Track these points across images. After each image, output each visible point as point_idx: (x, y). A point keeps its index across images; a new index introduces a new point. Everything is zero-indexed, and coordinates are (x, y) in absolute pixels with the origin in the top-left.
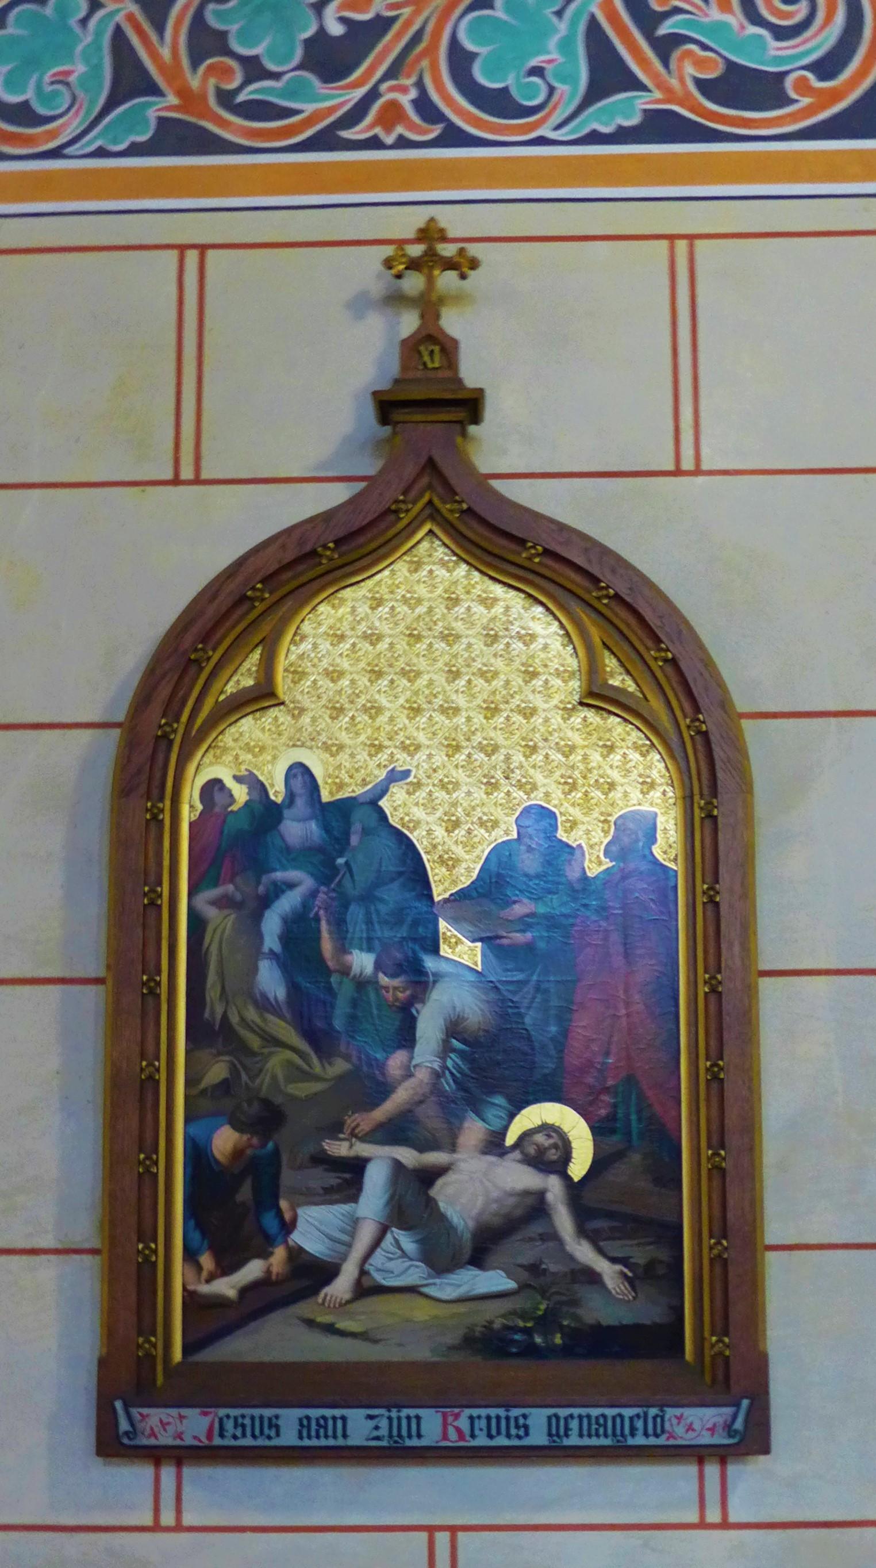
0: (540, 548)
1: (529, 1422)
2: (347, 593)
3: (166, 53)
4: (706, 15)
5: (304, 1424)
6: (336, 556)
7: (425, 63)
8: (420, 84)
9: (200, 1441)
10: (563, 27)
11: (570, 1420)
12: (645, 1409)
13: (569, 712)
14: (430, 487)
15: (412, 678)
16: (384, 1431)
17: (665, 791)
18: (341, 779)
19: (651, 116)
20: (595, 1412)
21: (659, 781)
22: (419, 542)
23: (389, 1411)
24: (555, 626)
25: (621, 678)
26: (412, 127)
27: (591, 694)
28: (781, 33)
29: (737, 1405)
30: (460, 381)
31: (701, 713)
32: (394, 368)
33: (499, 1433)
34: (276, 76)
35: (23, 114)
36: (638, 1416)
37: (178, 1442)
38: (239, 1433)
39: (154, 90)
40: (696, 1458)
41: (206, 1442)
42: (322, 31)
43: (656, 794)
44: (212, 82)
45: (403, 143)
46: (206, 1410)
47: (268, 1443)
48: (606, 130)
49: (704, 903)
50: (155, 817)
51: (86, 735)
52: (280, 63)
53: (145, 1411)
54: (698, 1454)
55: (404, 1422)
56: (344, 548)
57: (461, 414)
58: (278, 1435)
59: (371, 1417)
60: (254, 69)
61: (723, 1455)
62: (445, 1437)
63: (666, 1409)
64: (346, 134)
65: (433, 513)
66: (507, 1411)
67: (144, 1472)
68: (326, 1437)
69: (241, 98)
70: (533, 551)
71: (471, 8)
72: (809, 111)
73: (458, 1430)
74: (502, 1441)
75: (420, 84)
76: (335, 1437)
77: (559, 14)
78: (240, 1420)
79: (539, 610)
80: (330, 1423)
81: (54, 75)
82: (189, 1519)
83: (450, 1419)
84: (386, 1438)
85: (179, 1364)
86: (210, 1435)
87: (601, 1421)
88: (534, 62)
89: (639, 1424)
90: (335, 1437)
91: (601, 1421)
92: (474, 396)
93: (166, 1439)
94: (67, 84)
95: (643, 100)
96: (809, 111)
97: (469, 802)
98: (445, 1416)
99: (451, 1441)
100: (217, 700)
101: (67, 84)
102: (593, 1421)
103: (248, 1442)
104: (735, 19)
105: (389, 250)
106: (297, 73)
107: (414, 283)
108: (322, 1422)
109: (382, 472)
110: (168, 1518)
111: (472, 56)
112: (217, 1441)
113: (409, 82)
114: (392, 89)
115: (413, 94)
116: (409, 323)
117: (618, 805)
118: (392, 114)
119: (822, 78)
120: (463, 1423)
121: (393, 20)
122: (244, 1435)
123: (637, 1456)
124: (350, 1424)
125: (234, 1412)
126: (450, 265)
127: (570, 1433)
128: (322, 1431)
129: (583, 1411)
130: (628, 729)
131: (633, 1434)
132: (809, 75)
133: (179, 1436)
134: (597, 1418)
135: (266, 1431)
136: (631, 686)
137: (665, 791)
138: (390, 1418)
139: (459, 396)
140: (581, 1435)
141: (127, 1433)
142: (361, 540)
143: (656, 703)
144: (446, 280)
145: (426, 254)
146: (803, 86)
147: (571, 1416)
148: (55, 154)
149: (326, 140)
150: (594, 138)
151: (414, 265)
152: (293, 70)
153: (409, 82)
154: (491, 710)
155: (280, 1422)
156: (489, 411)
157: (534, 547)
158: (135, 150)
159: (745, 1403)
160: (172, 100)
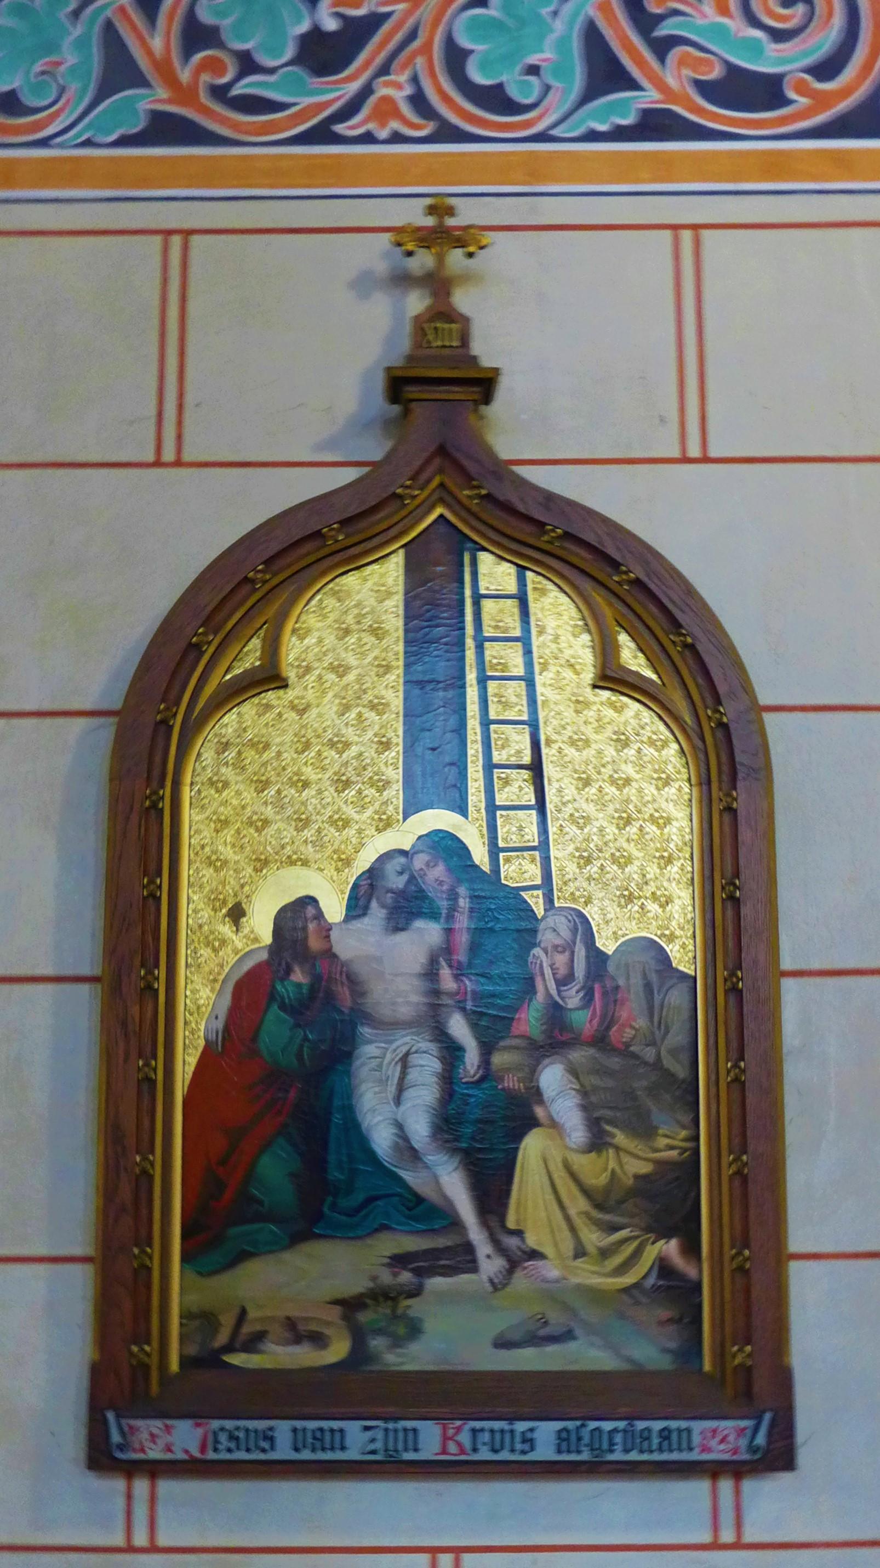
3: (157, 43)
5: (563, 1439)
8: (415, 80)
14: (441, 471)
15: (220, 789)
16: (379, 1445)
19: (647, 114)
20: (312, 1425)
28: (778, 36)
29: (759, 1419)
31: (722, 705)
32: (405, 345)
34: (272, 71)
37: (169, 1456)
41: (196, 1453)
44: (205, 78)
45: (397, 138)
46: (199, 1421)
48: (603, 127)
49: (723, 900)
50: (154, 805)
51: (81, 722)
53: (133, 1422)
54: (714, 1470)
58: (273, 1448)
59: (367, 1428)
60: (248, 65)
62: (444, 1452)
64: (340, 128)
67: (700, 1488)
69: (236, 91)
70: (553, 534)
71: (465, 8)
73: (459, 1444)
74: (505, 1455)
75: (415, 80)
77: (555, 13)
83: (451, 1432)
84: (382, 1452)
86: (203, 1449)
88: (533, 59)
91: (564, 1445)
92: (490, 375)
93: (155, 1453)
98: (445, 1429)
103: (242, 1455)
105: (428, 201)
106: (290, 68)
107: (423, 261)
109: (388, 458)
110: (727, 1536)
111: (467, 53)
112: (211, 1455)
113: (403, 78)
114: (387, 84)
115: (408, 90)
117: (632, 801)
118: (387, 110)
120: (465, 1438)
124: (421, 1437)
125: (229, 1424)
132: (807, 77)
133: (169, 1449)
136: (649, 674)
144: (456, 257)
147: (615, 1430)
148: (44, 143)
150: (593, 136)
153: (403, 78)
154: (343, 784)
155: (536, 1435)
157: (553, 531)
158: (123, 141)
159: (768, 1417)
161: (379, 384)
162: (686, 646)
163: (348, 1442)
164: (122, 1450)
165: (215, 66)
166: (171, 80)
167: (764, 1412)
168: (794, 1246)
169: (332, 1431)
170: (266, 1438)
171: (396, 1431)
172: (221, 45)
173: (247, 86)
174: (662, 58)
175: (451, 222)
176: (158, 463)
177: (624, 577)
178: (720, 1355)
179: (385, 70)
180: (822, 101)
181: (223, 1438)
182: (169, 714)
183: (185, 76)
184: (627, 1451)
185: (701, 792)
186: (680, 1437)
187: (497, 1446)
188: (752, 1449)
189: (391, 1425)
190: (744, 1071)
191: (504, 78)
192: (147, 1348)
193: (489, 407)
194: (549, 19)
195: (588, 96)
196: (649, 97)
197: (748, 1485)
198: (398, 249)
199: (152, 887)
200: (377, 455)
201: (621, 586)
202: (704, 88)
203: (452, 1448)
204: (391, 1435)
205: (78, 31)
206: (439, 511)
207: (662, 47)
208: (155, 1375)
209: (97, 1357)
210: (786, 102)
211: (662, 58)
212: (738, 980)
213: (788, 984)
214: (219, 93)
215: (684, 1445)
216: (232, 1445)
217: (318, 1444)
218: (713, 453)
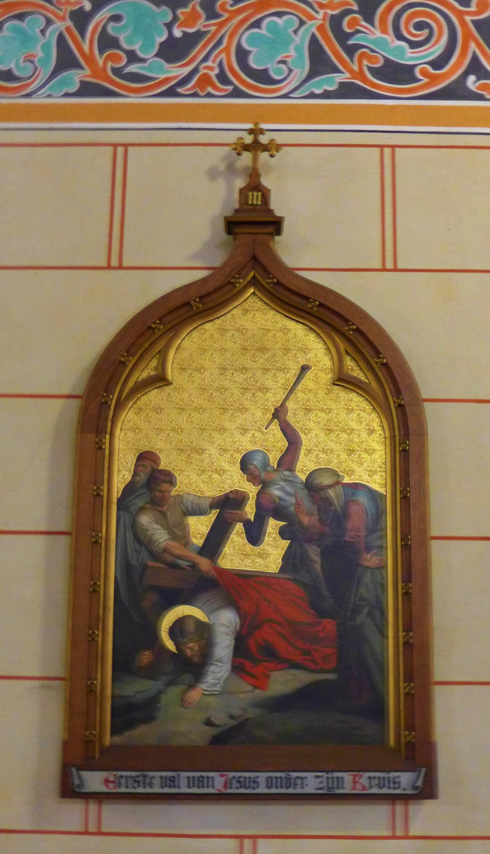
0: (317, 303)
2: (208, 326)
3: (86, 47)
4: (374, 34)
5: (269, 783)
7: (223, 56)
8: (220, 65)
10: (297, 39)
13: (329, 391)
14: (253, 268)
16: (325, 784)
18: (373, 427)
22: (247, 299)
25: (357, 372)
26: (215, 88)
27: (340, 380)
28: (413, 45)
29: (420, 772)
30: (271, 211)
34: (143, 60)
35: (8, 76)
39: (79, 66)
43: (376, 436)
44: (110, 64)
45: (209, 95)
47: (133, 791)
48: (318, 91)
54: (393, 799)
55: (335, 781)
57: (271, 229)
59: (318, 777)
60: (133, 57)
61: (406, 798)
64: (179, 90)
65: (254, 282)
69: (127, 70)
72: (426, 86)
75: (220, 65)
77: (296, 32)
84: (326, 789)
86: (225, 786)
88: (279, 58)
91: (201, 784)
92: (278, 220)
94: (32, 62)
95: (340, 78)
96: (426, 86)
97: (359, 439)
101: (32, 62)
102: (196, 779)
104: (390, 37)
107: (246, 158)
108: (201, 779)
111: (248, 53)
115: (217, 71)
116: (240, 183)
118: (205, 80)
119: (435, 68)
126: (265, 148)
128: (201, 784)
130: (361, 400)
138: (328, 778)
139: (274, 219)
143: (374, 385)
144: (264, 156)
148: (28, 95)
149: (171, 92)
150: (312, 96)
151: (246, 148)
152: (149, 59)
156: (286, 227)
158: (67, 95)
159: (423, 770)
160: (88, 72)
161: (221, 225)
162: (383, 364)
163: (216, 784)
165: (115, 58)
169: (208, 778)
170: (255, 782)
171: (332, 778)
172: (119, 47)
173: (134, 68)
174: (351, 57)
175: (264, 139)
176: (109, 267)
177: (351, 327)
178: (398, 736)
179: (205, 59)
180: (434, 79)
181: (234, 782)
185: (391, 440)
186: (208, 781)
187: (382, 785)
188: (415, 788)
189: (330, 775)
190: (411, 588)
191: (268, 66)
192: (94, 732)
194: (293, 34)
195: (311, 75)
196: (344, 77)
197: (413, 808)
200: (217, 264)
202: (374, 72)
204: (330, 780)
207: (351, 50)
208: (97, 746)
211: (351, 57)
212: (409, 540)
214: (117, 72)
216: (238, 785)
217: (172, 784)
218: (400, 266)
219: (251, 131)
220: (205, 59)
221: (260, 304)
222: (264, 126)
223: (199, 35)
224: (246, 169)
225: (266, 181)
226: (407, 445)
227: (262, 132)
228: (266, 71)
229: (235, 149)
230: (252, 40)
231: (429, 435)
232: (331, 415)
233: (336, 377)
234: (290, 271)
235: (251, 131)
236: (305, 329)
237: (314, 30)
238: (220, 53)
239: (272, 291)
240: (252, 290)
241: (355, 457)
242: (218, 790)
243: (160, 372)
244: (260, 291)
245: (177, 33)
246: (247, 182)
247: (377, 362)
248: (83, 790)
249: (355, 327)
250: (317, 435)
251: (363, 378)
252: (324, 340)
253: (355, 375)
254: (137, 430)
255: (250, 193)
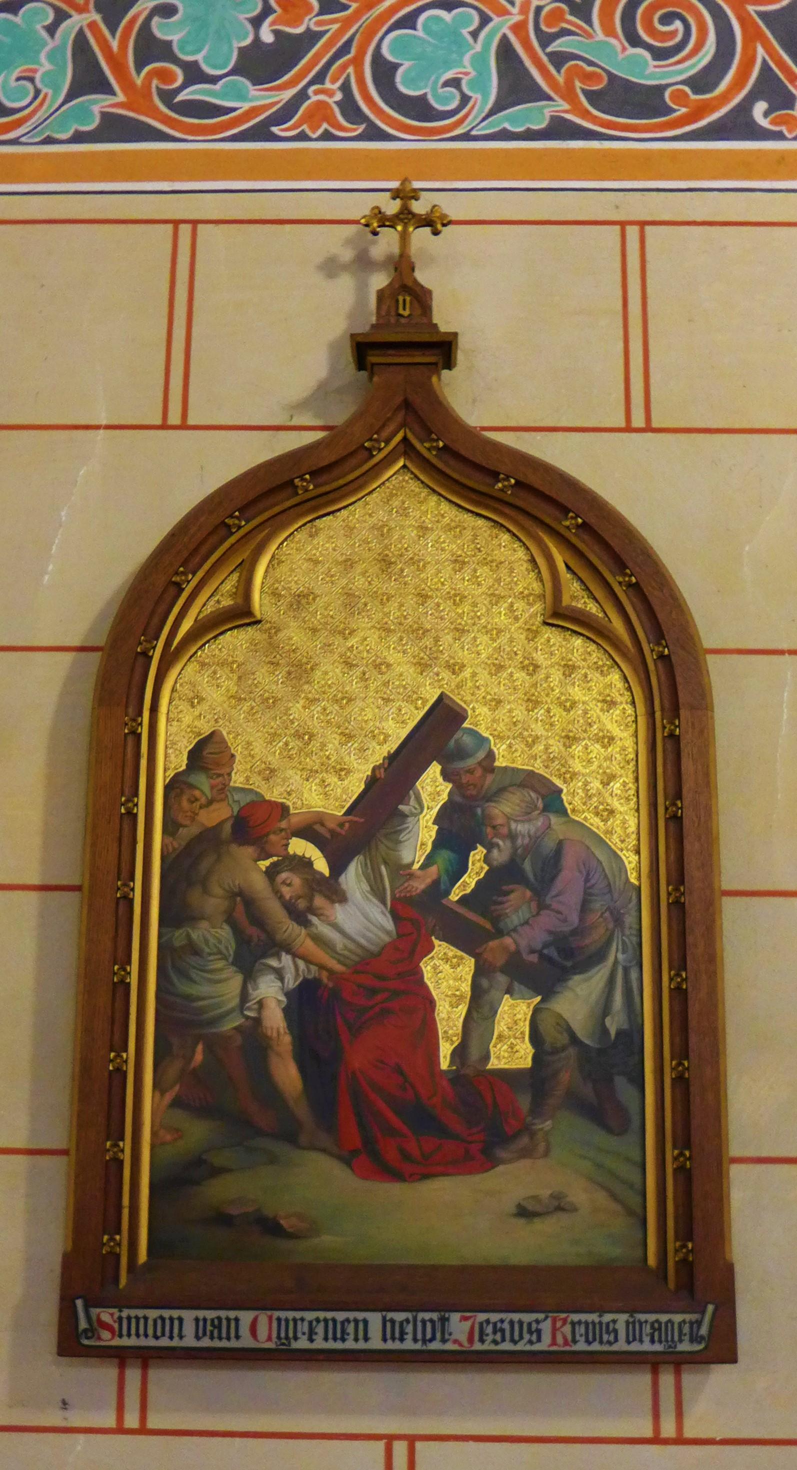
0: (513, 481)
1: (617, 1327)
6: (311, 487)
8: (346, 88)
9: (461, 1345)
11: (346, 1324)
12: (414, 1314)
14: (403, 425)
17: (624, 709)
21: (619, 699)
23: (121, 1311)
24: (521, 554)
27: (556, 614)
28: (659, 54)
29: (703, 1312)
33: (163, 1335)
34: (214, 80)
36: (407, 1321)
38: (498, 1337)
40: (649, 1366)
42: (257, 40)
45: (327, 136)
52: (215, 67)
56: (320, 480)
60: (194, 74)
62: (554, 1343)
63: (635, 1315)
64: (275, 130)
66: (600, 1316)
67: (108, 1373)
68: (220, 1338)
69: (181, 97)
76: (228, 1338)
77: (475, 34)
78: (499, 1325)
79: (505, 537)
80: (224, 1323)
81: (25, 71)
82: (153, 1423)
83: (559, 1324)
85: (145, 1264)
86: (471, 1340)
87: (216, 1322)
89: (409, 1329)
90: (228, 1338)
91: (216, 1322)
92: (450, 338)
99: (559, 1346)
100: (197, 618)
103: (507, 1346)
111: (395, 67)
112: (478, 1346)
114: (316, 93)
115: (339, 96)
116: (380, 281)
119: (696, 91)
121: (322, 34)
122: (616, 1340)
123: (195, 1358)
125: (494, 1317)
127: (405, 1337)
129: (329, 1315)
131: (343, 1340)
132: (687, 89)
134: (212, 1320)
135: (527, 1336)
136: (592, 608)
137: (624, 709)
140: (326, 1339)
141: (85, 1331)
142: (336, 472)
143: (618, 625)
144: (420, 236)
145: (401, 212)
146: (679, 97)
147: (348, 1320)
148: (15, 142)
149: (261, 133)
150: (504, 135)
158: (79, 138)
159: (710, 1308)
160: (121, 97)
164: (88, 1338)
166: (128, 85)
167: (707, 1303)
168: (735, 1150)
173: (194, 93)
175: (419, 207)
179: (320, 78)
181: (489, 1329)
182: (148, 646)
183: (139, 81)
184: (629, 1342)
193: (455, 371)
194: (470, 39)
197: (689, 1379)
198: (367, 228)
199: (130, 805)
201: (570, 530)
203: (560, 1340)
205: (51, 44)
206: (401, 463)
209: (69, 1249)
210: (670, 111)
213: (726, 901)
215: (233, 1334)
219: (396, 194)
220: (320, 78)
221: (414, 486)
222: (417, 185)
223: (312, 37)
224: (389, 259)
225: (422, 277)
226: (676, 727)
227: (415, 195)
228: (423, 99)
229: (367, 225)
230: (400, 47)
231: (715, 710)
232: (500, 640)
233: (549, 612)
234: (472, 435)
235: (396, 194)
236: (492, 526)
237: (505, 30)
238: (344, 67)
239: (435, 461)
240: (401, 463)
241: (541, 712)
242: (456, 1341)
243: (240, 601)
244: (412, 461)
245: (267, 36)
246: (390, 280)
247: (620, 583)
248: (676, 1350)
249: (580, 520)
250: (474, 675)
251: (594, 610)
252: (524, 544)
253: (579, 606)
254: (196, 701)
255: (401, 298)
